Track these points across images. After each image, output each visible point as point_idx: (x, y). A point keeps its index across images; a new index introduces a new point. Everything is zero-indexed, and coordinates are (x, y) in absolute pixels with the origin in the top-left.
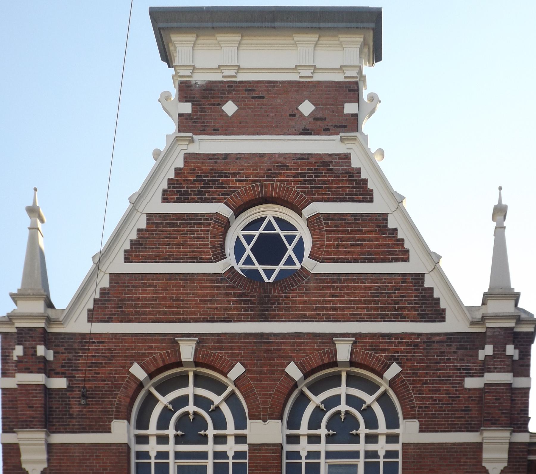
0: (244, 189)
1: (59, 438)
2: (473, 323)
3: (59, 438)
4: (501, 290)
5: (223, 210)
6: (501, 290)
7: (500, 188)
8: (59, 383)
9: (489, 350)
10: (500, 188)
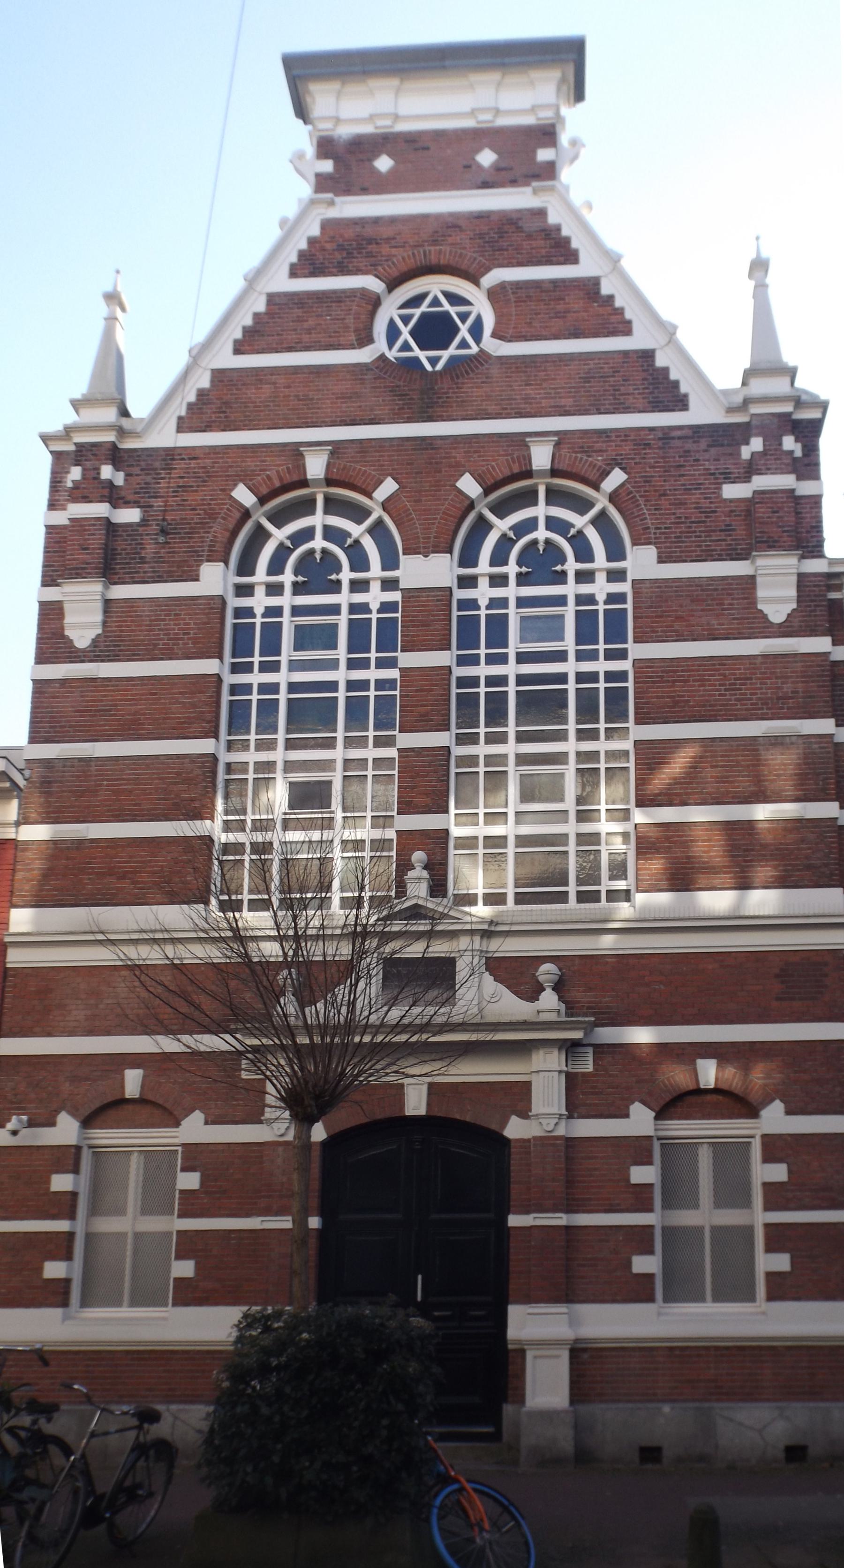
0: (402, 258)
1: (121, 592)
2: (730, 410)
3: (121, 592)
4: (767, 365)
5: (371, 283)
6: (767, 365)
7: (757, 238)
8: (130, 515)
9: (757, 444)
10: (757, 238)
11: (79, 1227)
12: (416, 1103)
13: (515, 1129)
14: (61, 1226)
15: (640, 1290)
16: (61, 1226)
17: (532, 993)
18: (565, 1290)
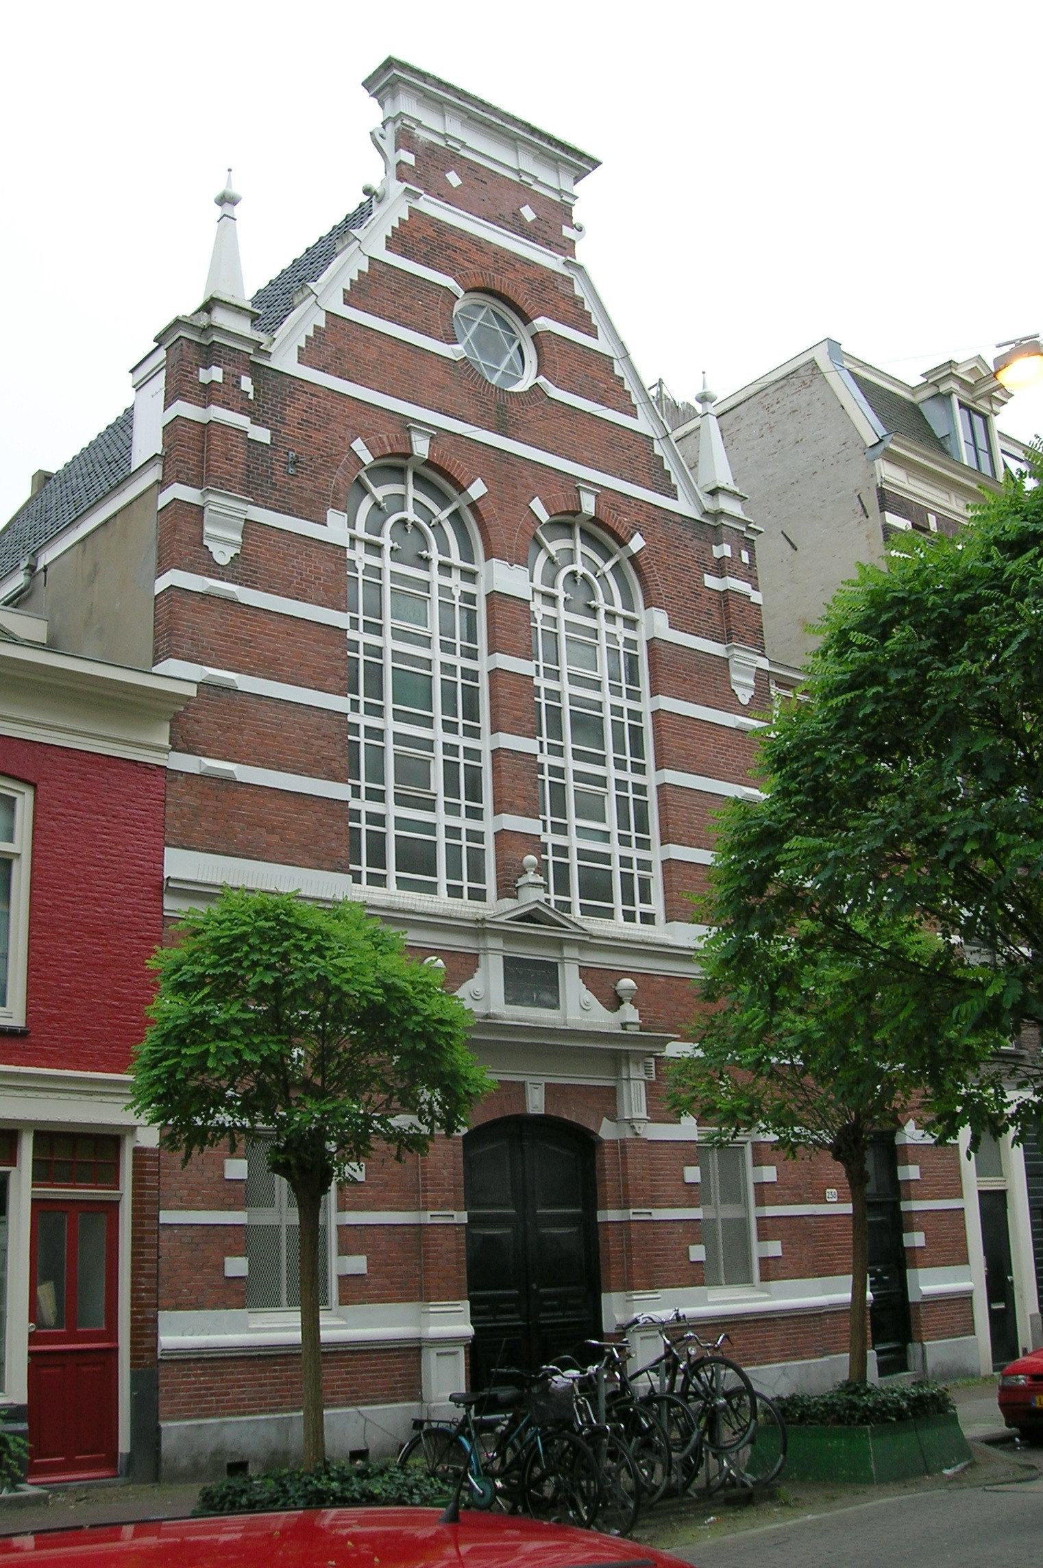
11: (754, 1212)
12: (536, 1103)
13: (607, 1131)
14: (771, 1211)
15: (696, 1276)
16: (771, 1211)
17: (614, 1002)
18: (652, 1279)
